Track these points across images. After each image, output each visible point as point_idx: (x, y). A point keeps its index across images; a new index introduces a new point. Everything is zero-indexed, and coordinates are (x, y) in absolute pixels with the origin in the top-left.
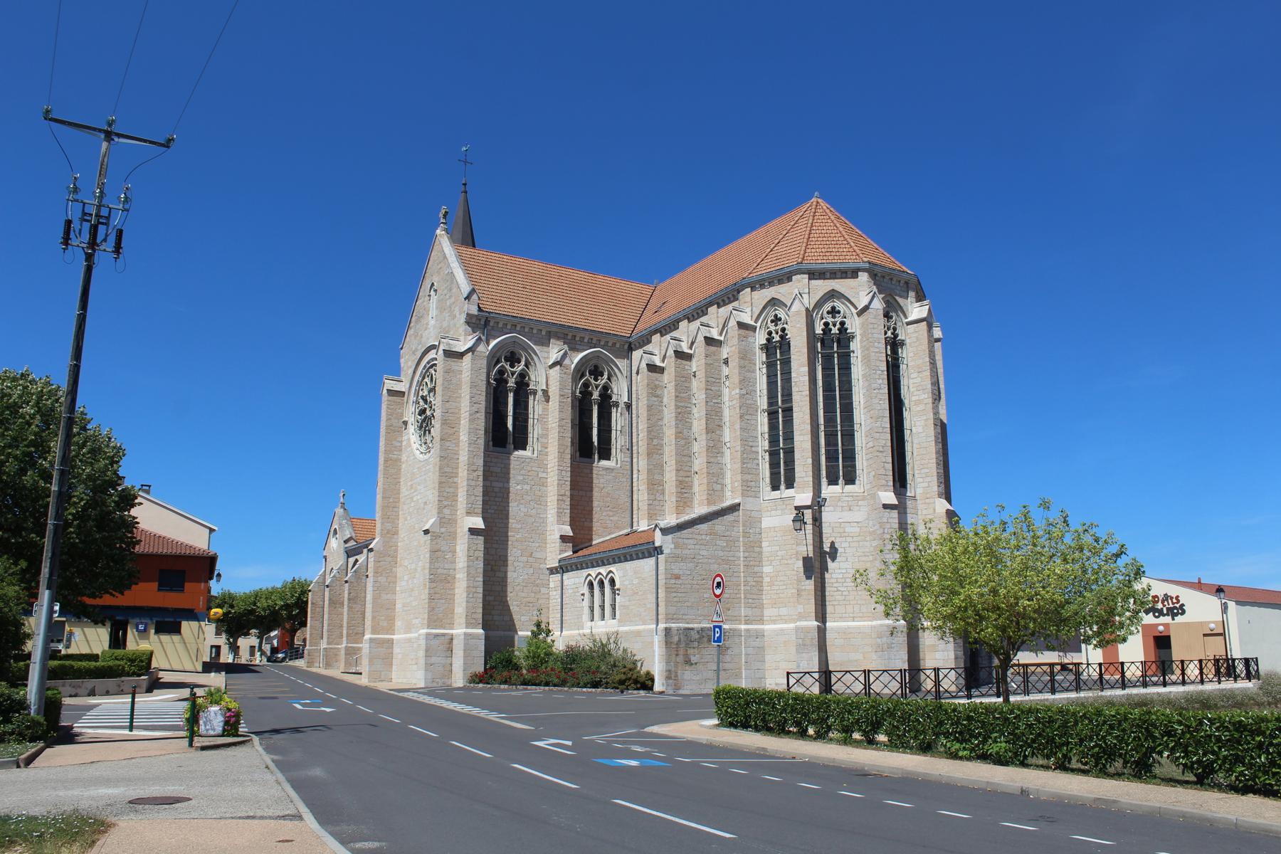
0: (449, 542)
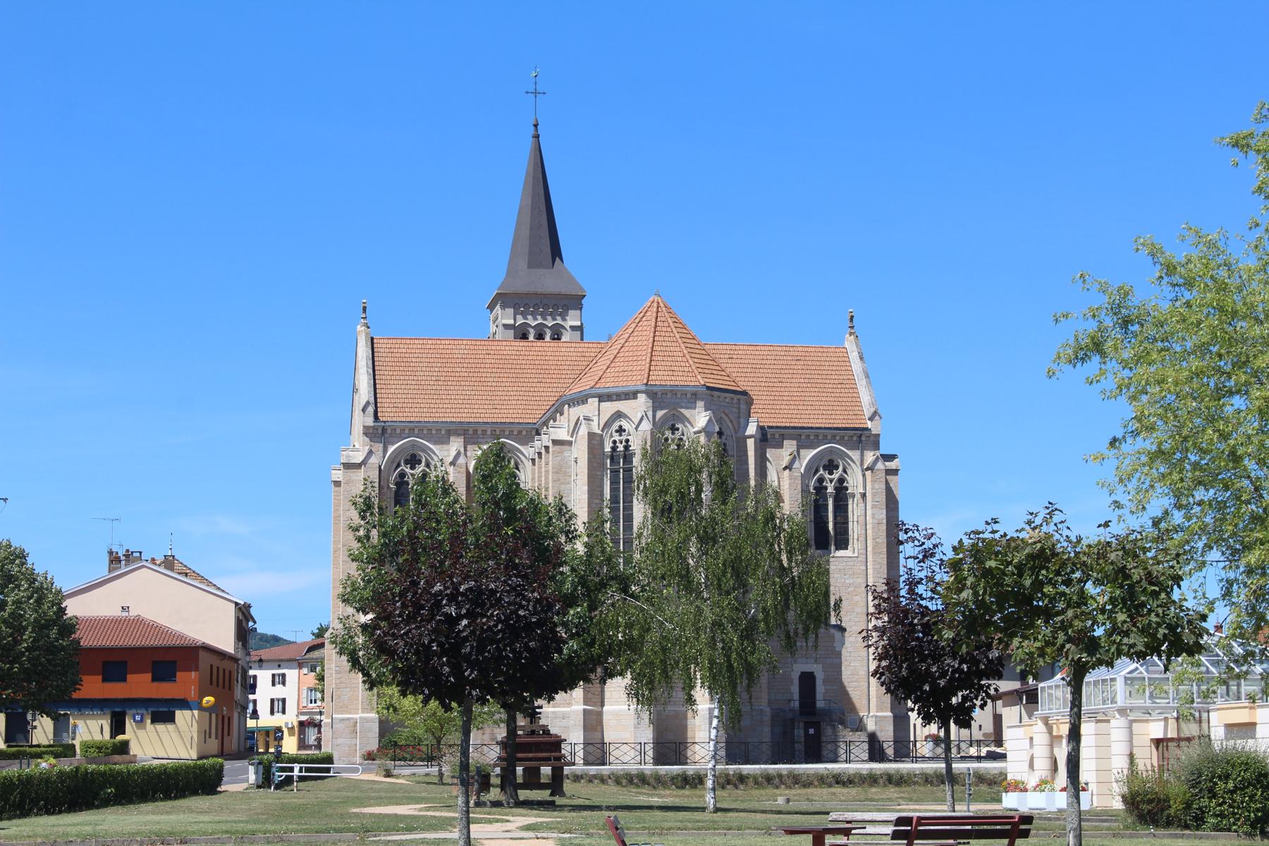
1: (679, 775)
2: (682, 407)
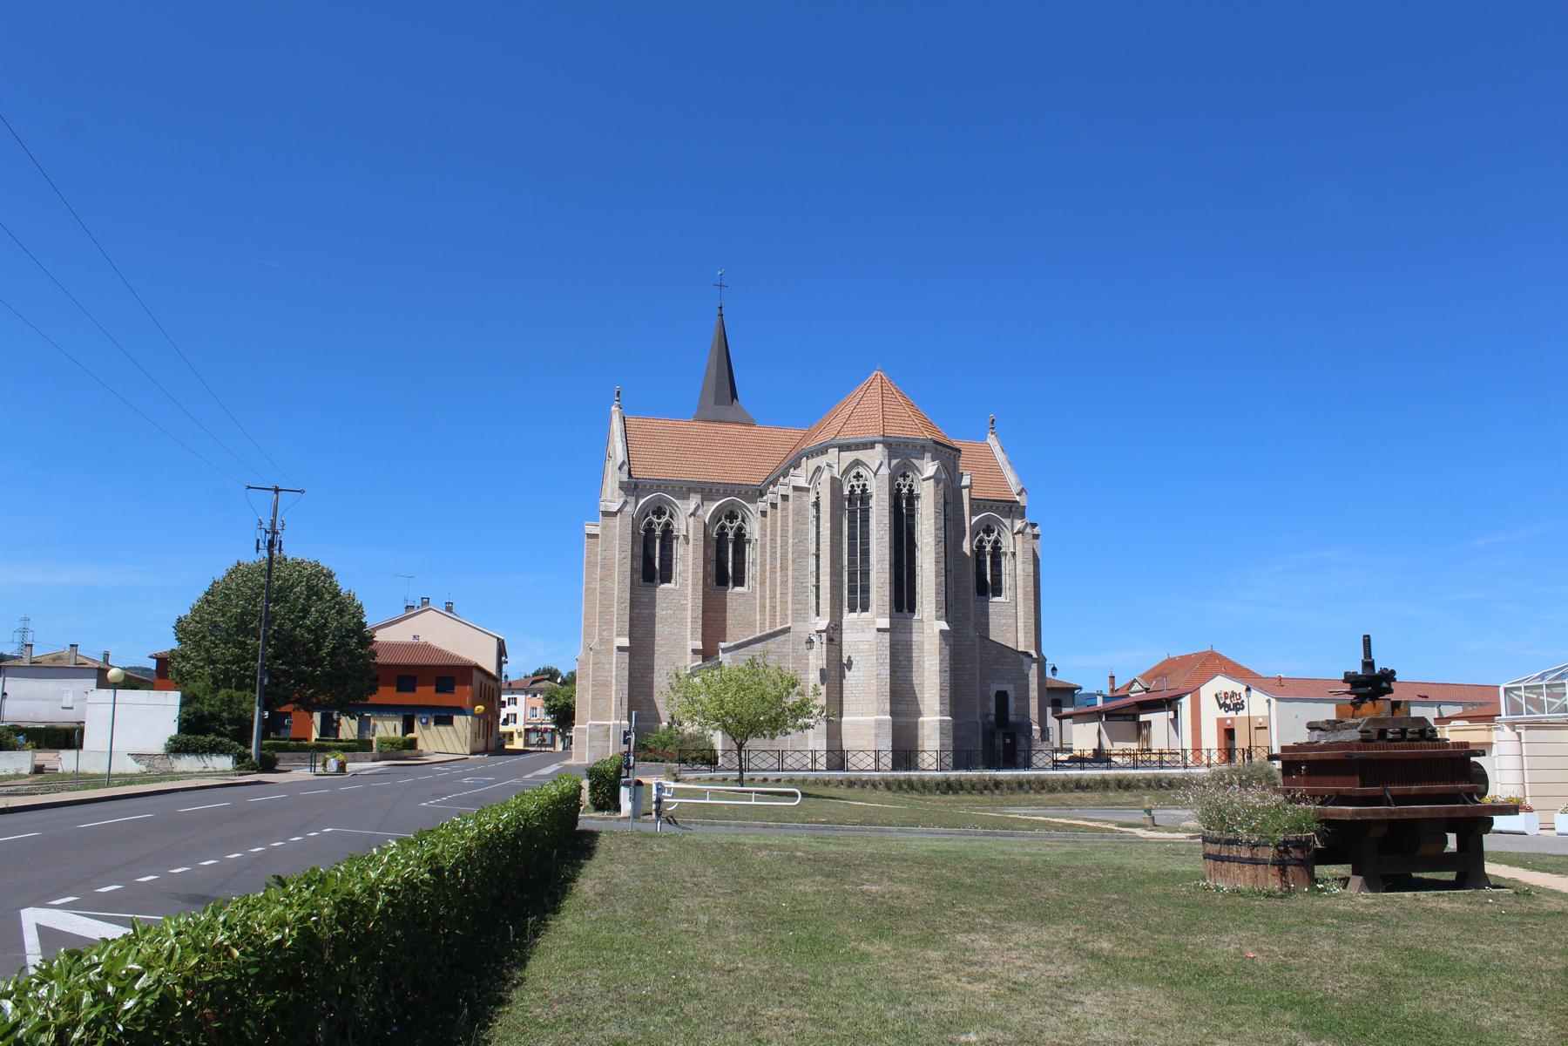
1: (943, 781)
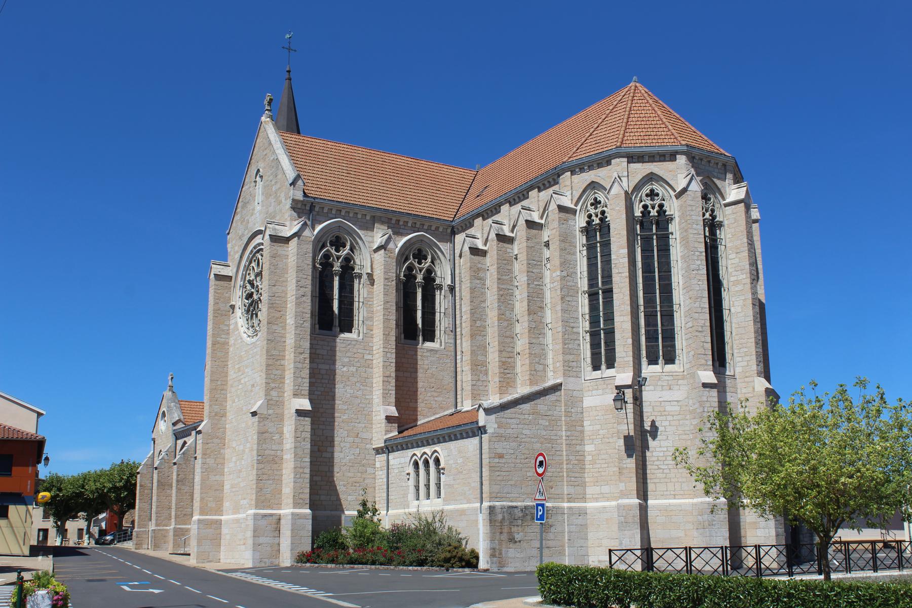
0: (276, 423)
2: (715, 177)
